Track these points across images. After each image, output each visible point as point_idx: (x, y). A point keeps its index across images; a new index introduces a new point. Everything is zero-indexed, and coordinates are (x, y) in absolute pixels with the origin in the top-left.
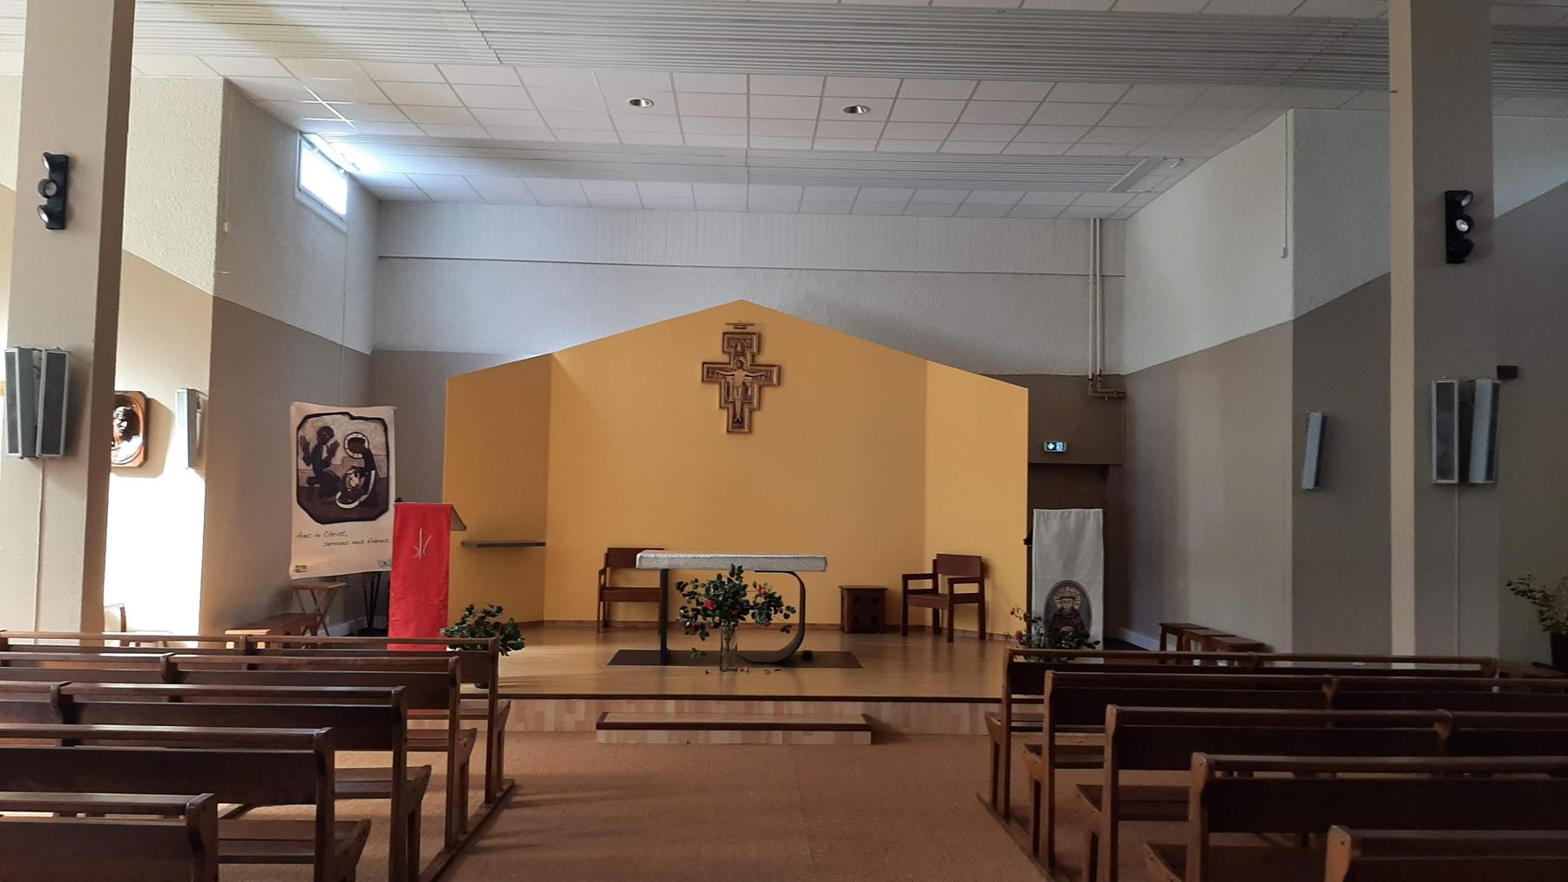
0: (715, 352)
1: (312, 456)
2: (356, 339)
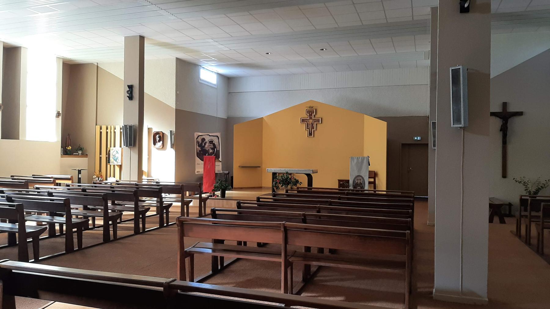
0: (305, 115)
1: (200, 145)
2: (222, 114)
